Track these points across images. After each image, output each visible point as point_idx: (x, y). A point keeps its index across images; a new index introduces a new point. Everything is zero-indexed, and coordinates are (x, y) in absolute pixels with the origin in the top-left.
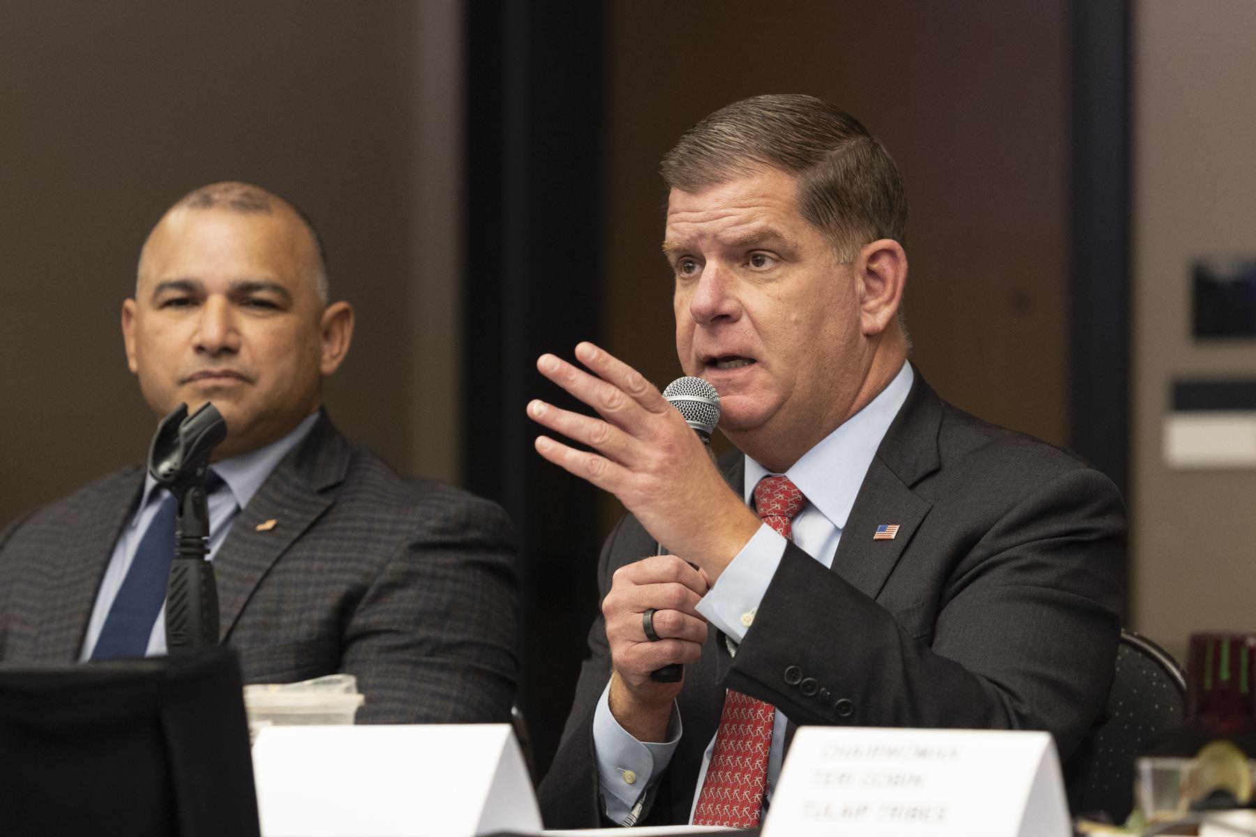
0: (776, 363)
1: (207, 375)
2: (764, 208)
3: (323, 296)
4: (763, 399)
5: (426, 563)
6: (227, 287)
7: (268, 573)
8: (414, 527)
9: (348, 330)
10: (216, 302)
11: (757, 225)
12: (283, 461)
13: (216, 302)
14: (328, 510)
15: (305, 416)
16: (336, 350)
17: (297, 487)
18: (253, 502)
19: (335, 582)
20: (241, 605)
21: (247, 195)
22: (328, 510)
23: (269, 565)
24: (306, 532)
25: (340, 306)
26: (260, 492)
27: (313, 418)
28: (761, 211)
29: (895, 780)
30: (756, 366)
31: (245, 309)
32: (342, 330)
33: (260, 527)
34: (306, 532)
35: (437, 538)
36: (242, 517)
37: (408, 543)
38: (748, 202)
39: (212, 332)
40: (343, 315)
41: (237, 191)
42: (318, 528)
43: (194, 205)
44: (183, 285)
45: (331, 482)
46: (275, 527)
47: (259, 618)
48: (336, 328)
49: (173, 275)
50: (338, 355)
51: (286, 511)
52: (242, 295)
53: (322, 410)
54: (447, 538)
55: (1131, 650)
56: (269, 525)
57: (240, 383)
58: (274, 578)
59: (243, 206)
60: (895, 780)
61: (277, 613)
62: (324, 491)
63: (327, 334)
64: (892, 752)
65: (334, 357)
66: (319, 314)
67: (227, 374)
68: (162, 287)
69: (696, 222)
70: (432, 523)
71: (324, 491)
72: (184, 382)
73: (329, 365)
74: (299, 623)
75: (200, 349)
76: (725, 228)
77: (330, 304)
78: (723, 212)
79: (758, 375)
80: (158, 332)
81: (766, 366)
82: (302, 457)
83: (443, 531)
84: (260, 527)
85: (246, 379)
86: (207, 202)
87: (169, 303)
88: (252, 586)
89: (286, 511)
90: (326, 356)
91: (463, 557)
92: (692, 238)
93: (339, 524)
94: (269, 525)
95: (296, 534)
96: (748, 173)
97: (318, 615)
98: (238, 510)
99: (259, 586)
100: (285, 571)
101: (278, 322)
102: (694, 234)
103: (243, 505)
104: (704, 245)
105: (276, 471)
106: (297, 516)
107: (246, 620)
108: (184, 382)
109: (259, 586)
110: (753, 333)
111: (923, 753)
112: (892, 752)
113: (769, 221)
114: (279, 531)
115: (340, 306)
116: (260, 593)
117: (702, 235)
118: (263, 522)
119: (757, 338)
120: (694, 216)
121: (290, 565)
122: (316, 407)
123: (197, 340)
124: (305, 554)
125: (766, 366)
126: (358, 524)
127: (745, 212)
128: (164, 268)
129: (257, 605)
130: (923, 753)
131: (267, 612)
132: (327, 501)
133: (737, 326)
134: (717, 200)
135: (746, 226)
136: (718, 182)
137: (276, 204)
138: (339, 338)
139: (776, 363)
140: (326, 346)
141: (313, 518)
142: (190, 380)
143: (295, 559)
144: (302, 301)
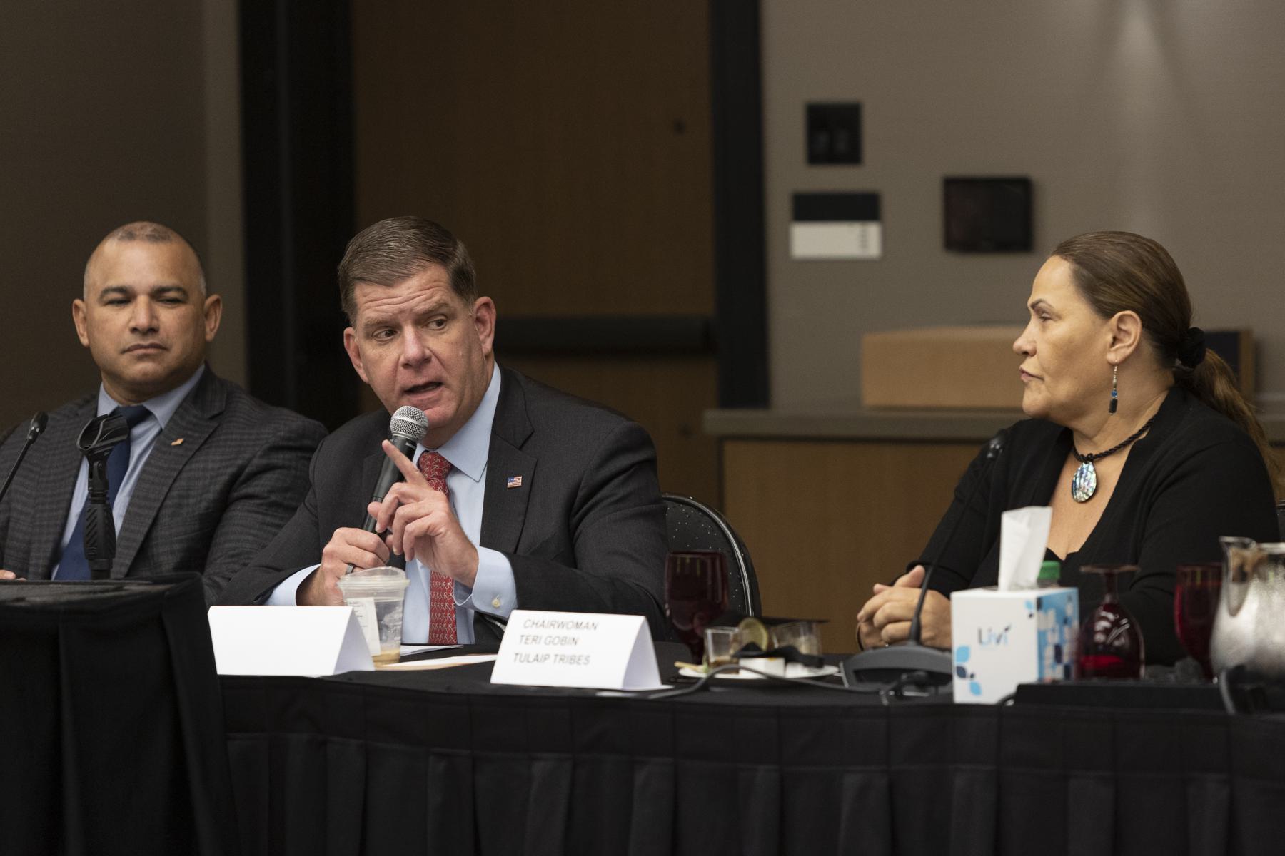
0: (455, 383)
1: (139, 347)
2: (437, 288)
3: (204, 291)
4: (450, 407)
5: (278, 458)
6: (149, 290)
7: (181, 472)
8: (270, 436)
9: (219, 312)
10: (142, 300)
11: (436, 298)
12: (185, 400)
13: (142, 300)
14: (216, 429)
15: (198, 366)
16: (212, 326)
17: (195, 416)
18: (167, 425)
19: (221, 475)
20: (165, 493)
21: (154, 230)
22: (216, 429)
23: (181, 467)
24: (203, 445)
25: (213, 298)
26: (172, 419)
27: (202, 368)
28: (437, 290)
29: (563, 641)
30: (442, 388)
31: (160, 304)
32: (215, 312)
33: (173, 444)
34: (199, 450)
35: (285, 443)
36: (162, 437)
37: (268, 445)
38: (428, 286)
39: (142, 320)
40: (217, 301)
41: (149, 228)
42: (210, 441)
43: (121, 238)
44: (121, 290)
45: (216, 412)
46: (183, 443)
47: (176, 501)
48: (212, 312)
49: (113, 283)
50: (214, 328)
51: (190, 433)
52: (158, 295)
53: (206, 363)
54: (291, 443)
55: (663, 606)
56: (179, 442)
57: (160, 351)
58: (184, 475)
59: (154, 238)
60: (563, 641)
61: (188, 497)
62: (213, 418)
63: (207, 315)
64: (562, 625)
65: (212, 330)
66: (203, 303)
67: (152, 346)
68: (107, 291)
69: (397, 304)
70: (282, 434)
71: (213, 418)
72: (124, 352)
73: (210, 336)
74: (201, 501)
75: (134, 330)
76: (418, 304)
77: (208, 296)
78: (414, 295)
79: (446, 393)
80: (106, 321)
81: (448, 387)
82: (196, 397)
83: (289, 439)
84: (173, 444)
85: (163, 348)
86: (131, 236)
87: (111, 302)
88: (170, 481)
89: (190, 433)
90: (208, 330)
91: (300, 454)
92: (394, 314)
93: (222, 438)
94: (179, 442)
95: (197, 447)
96: (424, 269)
97: (211, 496)
98: (161, 431)
99: (175, 480)
100: (191, 470)
101: (181, 310)
102: (396, 312)
103: (163, 427)
104: (401, 318)
105: (181, 406)
106: (197, 435)
107: (168, 502)
108: (124, 352)
109: (175, 480)
110: (440, 367)
111: (578, 626)
112: (562, 625)
113: (442, 295)
114: (186, 445)
115: (213, 298)
116: (177, 485)
117: (402, 312)
118: (176, 440)
119: (443, 370)
120: (395, 300)
121: (193, 466)
122: (203, 361)
123: (133, 324)
124: (202, 458)
125: (448, 387)
126: (234, 437)
127: (428, 293)
128: (106, 279)
129: (174, 493)
130: (578, 626)
131: (181, 497)
132: (215, 424)
133: (432, 364)
134: (409, 288)
135: (430, 301)
136: (408, 277)
137: (173, 235)
138: (214, 317)
139: (455, 383)
140: (206, 323)
141: (207, 436)
142: (129, 350)
143: (196, 462)
144: (194, 297)
